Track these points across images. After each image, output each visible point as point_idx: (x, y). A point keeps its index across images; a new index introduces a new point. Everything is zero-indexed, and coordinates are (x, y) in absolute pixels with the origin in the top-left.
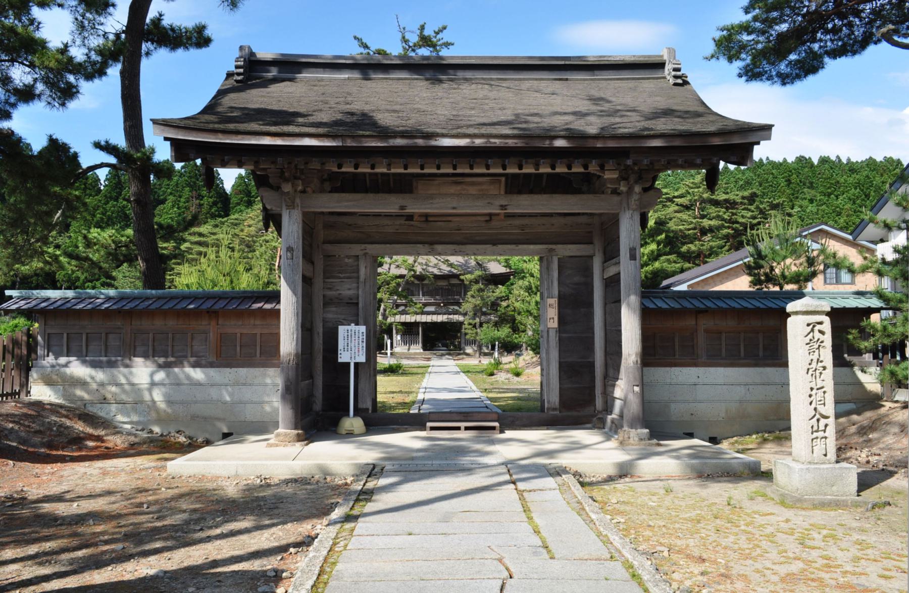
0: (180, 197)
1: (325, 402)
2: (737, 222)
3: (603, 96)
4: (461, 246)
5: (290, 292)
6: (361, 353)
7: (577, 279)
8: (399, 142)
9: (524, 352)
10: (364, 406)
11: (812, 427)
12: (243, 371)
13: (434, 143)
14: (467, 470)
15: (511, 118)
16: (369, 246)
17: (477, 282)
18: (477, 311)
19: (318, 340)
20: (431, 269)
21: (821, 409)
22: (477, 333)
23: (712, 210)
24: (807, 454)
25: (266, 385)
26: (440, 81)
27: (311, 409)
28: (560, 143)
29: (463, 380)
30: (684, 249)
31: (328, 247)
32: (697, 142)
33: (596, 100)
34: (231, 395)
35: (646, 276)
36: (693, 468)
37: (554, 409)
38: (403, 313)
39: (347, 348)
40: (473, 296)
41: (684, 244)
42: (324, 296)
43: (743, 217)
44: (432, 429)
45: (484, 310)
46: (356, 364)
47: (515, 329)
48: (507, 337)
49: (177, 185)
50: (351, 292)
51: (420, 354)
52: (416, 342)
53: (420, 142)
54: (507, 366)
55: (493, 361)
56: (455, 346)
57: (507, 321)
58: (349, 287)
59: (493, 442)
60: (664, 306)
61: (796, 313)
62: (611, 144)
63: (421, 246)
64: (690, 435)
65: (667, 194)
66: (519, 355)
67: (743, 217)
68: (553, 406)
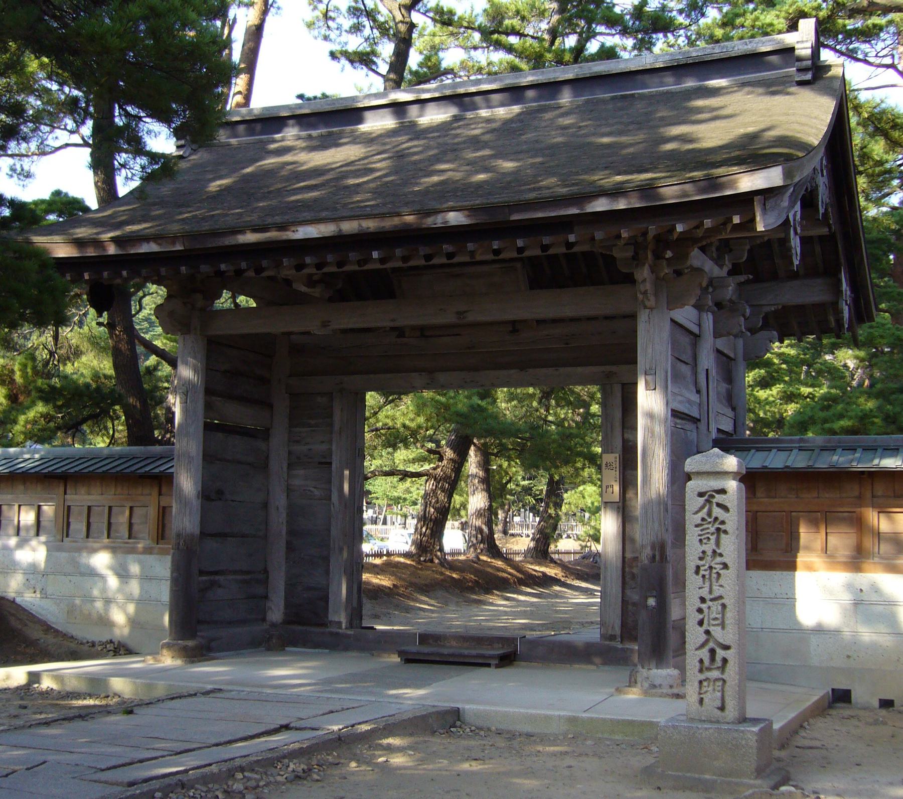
11: (701, 661)
13: (229, 241)
42: (290, 453)
61: (699, 474)
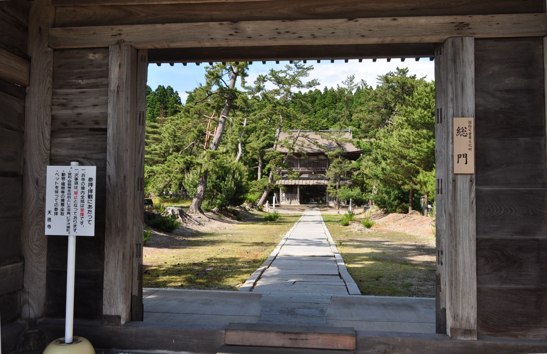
0: (154, 108)
4: (289, 23)
6: (86, 217)
7: (510, 82)
9: (370, 206)
10: (113, 312)
16: (127, 29)
17: (337, 157)
18: (337, 178)
20: (305, 149)
22: (336, 193)
27: (19, 316)
31: (57, 32)
37: (468, 332)
38: (287, 178)
40: (334, 167)
42: (53, 118)
45: (342, 176)
46: (80, 240)
47: (364, 189)
49: (153, 100)
50: (96, 111)
51: (298, 206)
52: (295, 199)
55: (347, 213)
56: (323, 201)
57: (358, 184)
58: (95, 101)
63: (216, 24)
66: (366, 209)
68: (465, 326)
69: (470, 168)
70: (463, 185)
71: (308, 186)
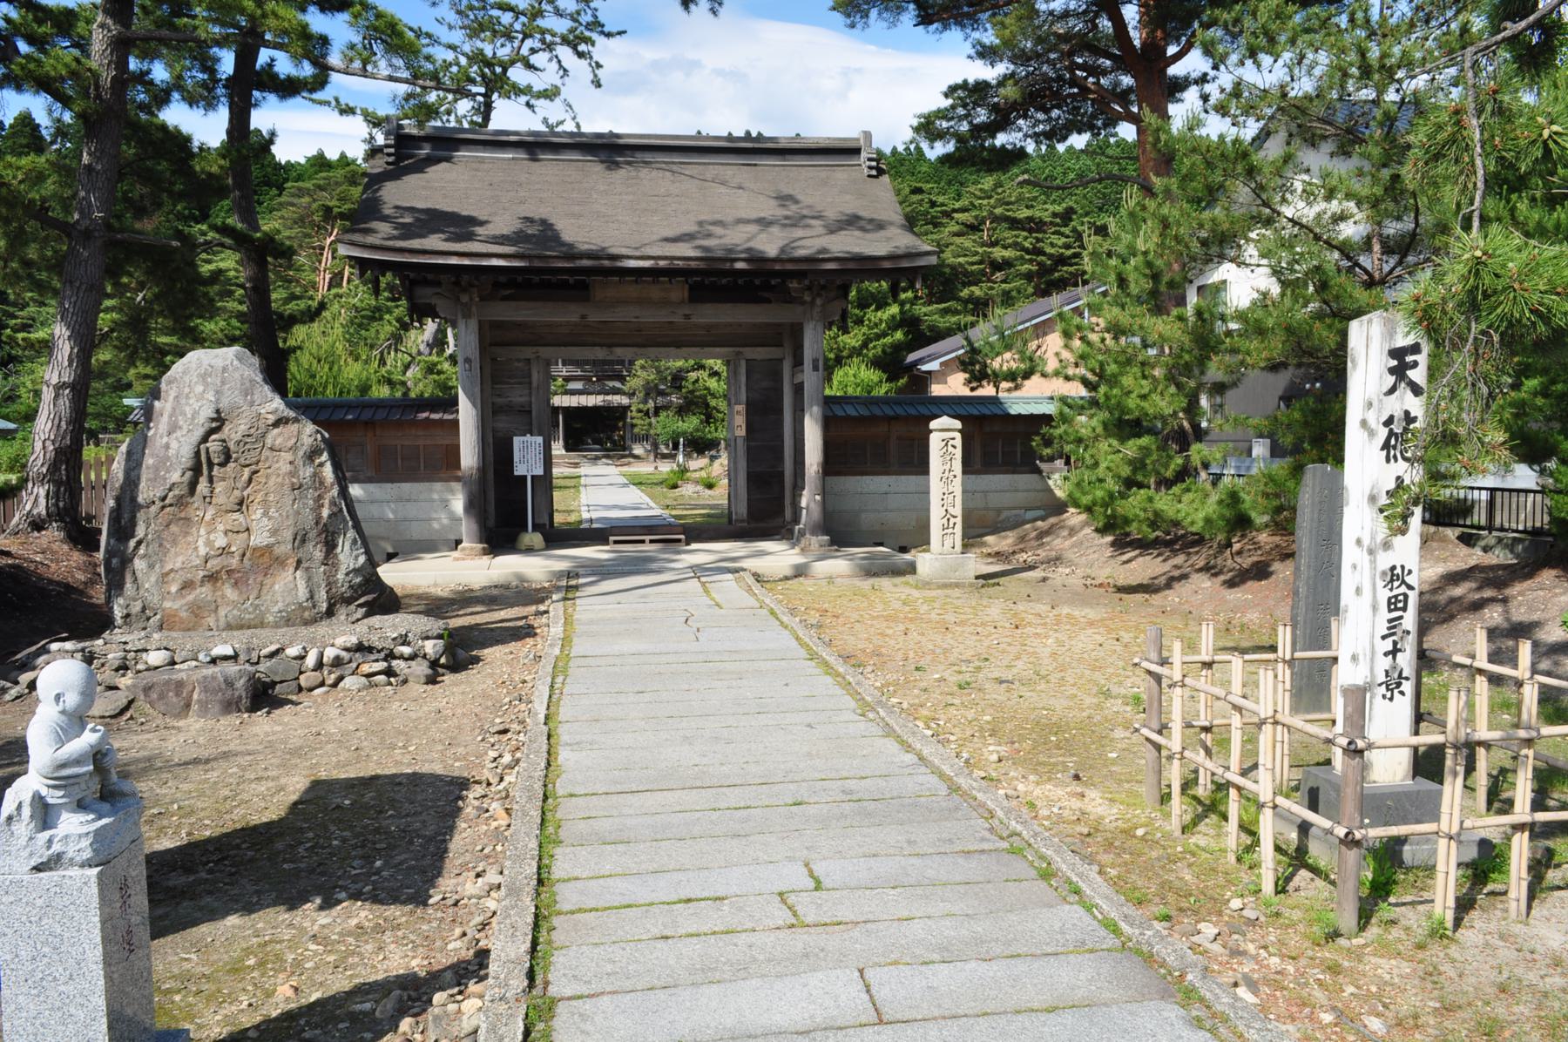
1: (508, 514)
2: (1044, 254)
3: (791, 192)
5: (469, 405)
8: (586, 263)
12: (406, 487)
14: (658, 572)
15: (694, 228)
16: (541, 349)
18: (651, 391)
19: (498, 453)
21: (951, 510)
22: (650, 424)
23: (1009, 235)
24: (942, 553)
25: (433, 501)
26: (617, 165)
28: (740, 265)
29: (635, 495)
30: (965, 293)
32: (869, 266)
33: (785, 199)
34: (394, 512)
35: (884, 351)
36: (861, 567)
39: (523, 460)
41: (965, 285)
43: (1052, 245)
44: (616, 542)
47: (709, 417)
48: (697, 430)
53: (606, 263)
54: (697, 475)
56: (613, 442)
57: (696, 404)
59: (679, 553)
60: (854, 413)
62: (789, 267)
64: (881, 544)
65: (943, 205)
66: (713, 458)
67: (1052, 245)
69: (743, 433)
70: (740, 443)
71: (585, 408)
